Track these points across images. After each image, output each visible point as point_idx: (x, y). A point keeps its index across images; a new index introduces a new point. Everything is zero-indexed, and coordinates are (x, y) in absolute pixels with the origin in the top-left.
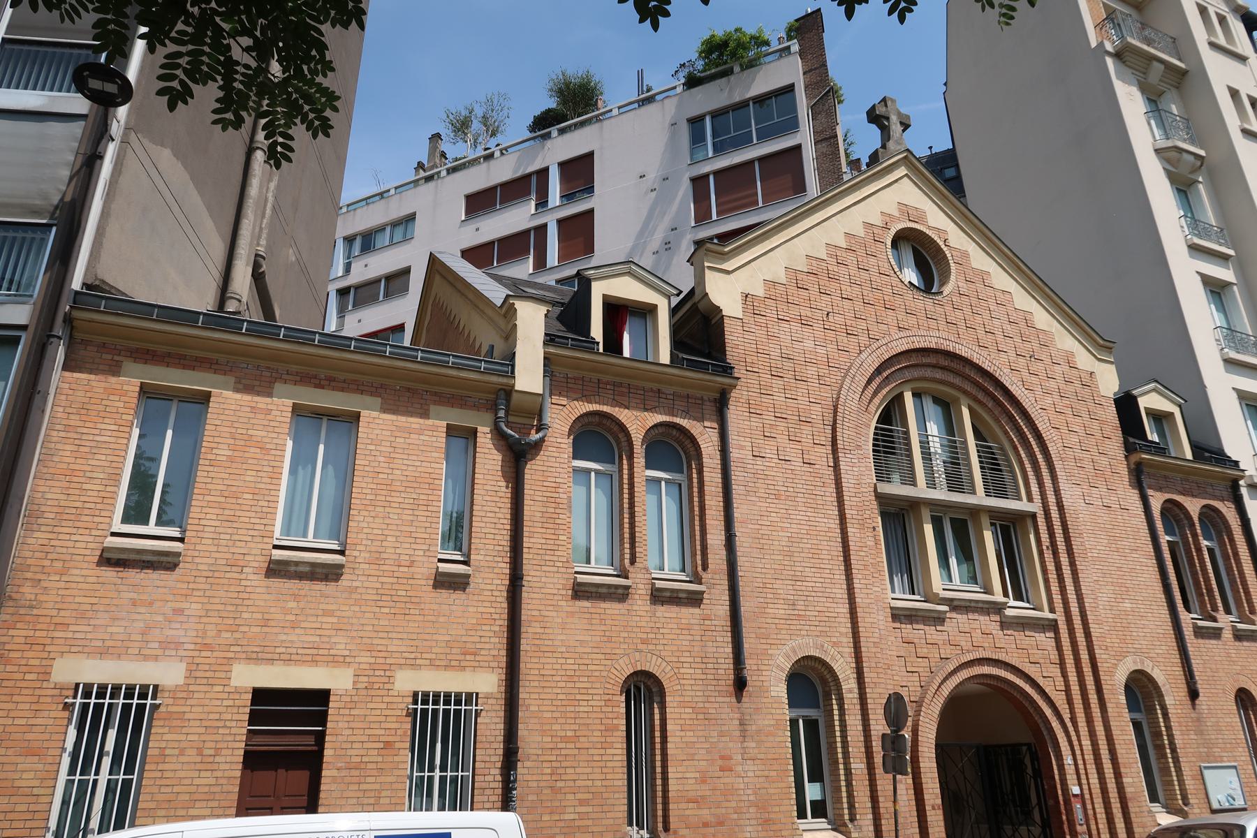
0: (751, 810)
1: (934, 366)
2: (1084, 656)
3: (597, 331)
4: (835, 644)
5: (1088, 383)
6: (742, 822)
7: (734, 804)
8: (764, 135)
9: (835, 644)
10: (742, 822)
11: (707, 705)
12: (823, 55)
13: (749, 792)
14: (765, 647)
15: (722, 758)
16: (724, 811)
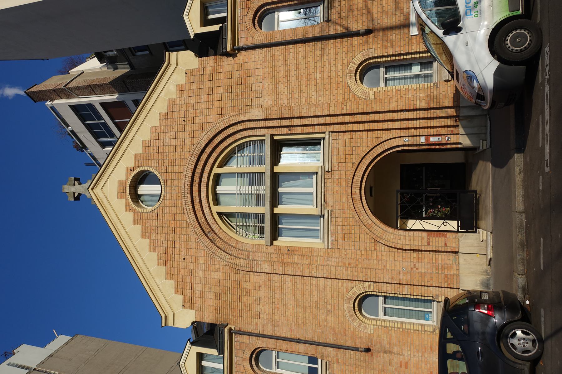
0: (426, 356)
1: (200, 191)
2: (348, 119)
3: (216, 28)
4: (347, 291)
5: (192, 76)
6: (431, 362)
7: (423, 365)
8: (100, 117)
9: (347, 291)
10: (431, 362)
11: (377, 369)
12: (49, 91)
13: (417, 355)
14: (350, 332)
15: (401, 366)
16: (426, 370)
